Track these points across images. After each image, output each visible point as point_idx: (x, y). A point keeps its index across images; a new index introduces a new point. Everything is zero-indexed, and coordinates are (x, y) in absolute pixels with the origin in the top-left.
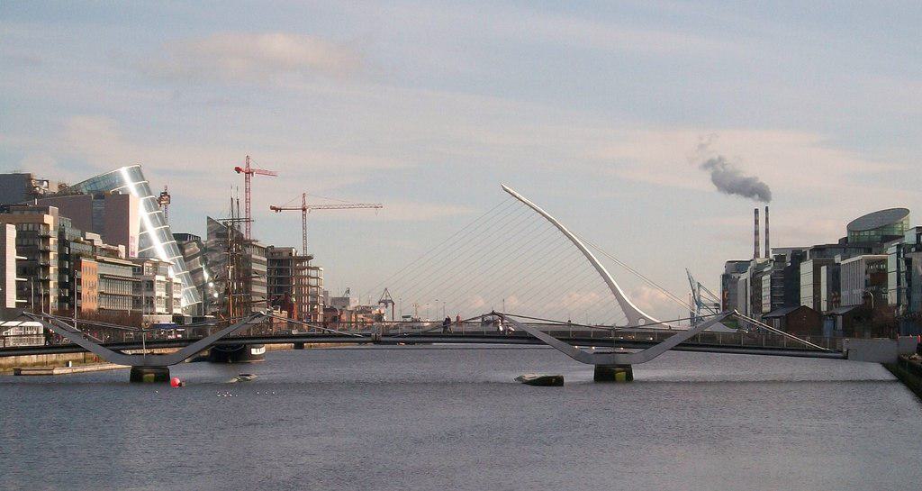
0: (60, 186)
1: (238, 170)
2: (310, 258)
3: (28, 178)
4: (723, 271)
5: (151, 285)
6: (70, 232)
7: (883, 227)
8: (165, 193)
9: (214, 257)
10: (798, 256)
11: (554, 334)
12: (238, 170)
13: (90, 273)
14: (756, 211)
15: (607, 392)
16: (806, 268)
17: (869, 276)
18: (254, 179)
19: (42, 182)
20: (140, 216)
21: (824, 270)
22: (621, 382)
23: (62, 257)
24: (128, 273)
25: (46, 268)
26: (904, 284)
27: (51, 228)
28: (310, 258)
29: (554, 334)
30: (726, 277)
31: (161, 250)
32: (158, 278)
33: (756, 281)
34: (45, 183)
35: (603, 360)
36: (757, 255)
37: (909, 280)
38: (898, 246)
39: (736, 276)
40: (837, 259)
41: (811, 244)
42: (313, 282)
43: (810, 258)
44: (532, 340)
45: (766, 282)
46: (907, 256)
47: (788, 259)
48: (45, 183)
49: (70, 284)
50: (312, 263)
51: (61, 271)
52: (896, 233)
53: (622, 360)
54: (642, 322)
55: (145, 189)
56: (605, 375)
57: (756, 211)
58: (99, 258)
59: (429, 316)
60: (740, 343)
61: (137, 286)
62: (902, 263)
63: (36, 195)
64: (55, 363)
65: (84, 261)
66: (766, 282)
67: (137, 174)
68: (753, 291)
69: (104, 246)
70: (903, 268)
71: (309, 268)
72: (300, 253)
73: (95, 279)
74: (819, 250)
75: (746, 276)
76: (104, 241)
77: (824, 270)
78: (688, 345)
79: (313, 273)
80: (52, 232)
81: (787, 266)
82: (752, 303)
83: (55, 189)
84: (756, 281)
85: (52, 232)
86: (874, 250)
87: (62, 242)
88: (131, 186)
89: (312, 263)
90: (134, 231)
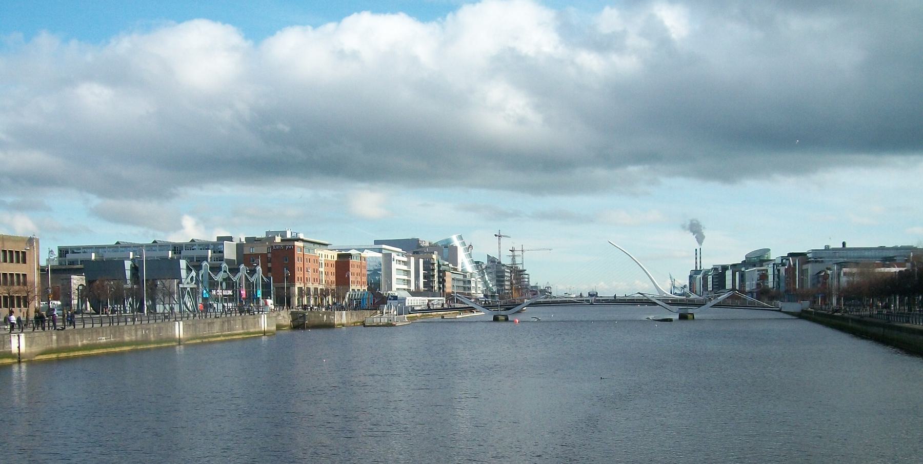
0: (429, 243)
1: (496, 236)
2: (525, 270)
3: (418, 240)
4: (689, 274)
5: (469, 282)
6: (441, 262)
7: (760, 256)
8: (471, 245)
9: (489, 270)
10: (725, 268)
11: (663, 301)
12: (496, 236)
13: (449, 277)
14: (696, 250)
15: (684, 324)
16: (729, 273)
17: (759, 276)
18: (502, 239)
19: (423, 241)
20: (462, 257)
21: (737, 273)
22: (502, 321)
23: (439, 271)
24: (461, 277)
25: (434, 275)
26: (776, 279)
27: (435, 260)
28: (525, 270)
29: (663, 301)
30: (691, 277)
31: (470, 268)
32: (473, 279)
33: (705, 278)
34: (424, 242)
35: (682, 312)
36: (696, 267)
37: (779, 277)
38: (774, 264)
39: (695, 276)
40: (743, 269)
41: (731, 263)
42: (526, 280)
43: (731, 269)
44: (655, 304)
45: (710, 279)
46: (778, 268)
47: (720, 269)
48: (424, 242)
49: (442, 281)
50: (526, 272)
51: (439, 277)
52: (765, 259)
53: (690, 311)
54: (665, 295)
55: (464, 244)
56: (683, 317)
57: (696, 250)
58: (452, 271)
59: (609, 294)
60: (755, 304)
61: (464, 282)
62: (776, 271)
63: (421, 247)
64: (446, 314)
65: (447, 273)
66: (710, 279)
67: (460, 238)
68: (703, 282)
69: (452, 267)
70: (776, 272)
71: (525, 274)
72: (521, 269)
73: (451, 280)
74: (734, 266)
75: (700, 276)
76: (453, 265)
77: (737, 273)
78: (532, 304)
79: (526, 276)
80: (436, 262)
81: (719, 274)
82: (703, 287)
83: (427, 244)
84: (705, 278)
85: (436, 262)
86: (757, 265)
87: (439, 266)
88: (456, 242)
89: (526, 272)
90: (459, 261)
